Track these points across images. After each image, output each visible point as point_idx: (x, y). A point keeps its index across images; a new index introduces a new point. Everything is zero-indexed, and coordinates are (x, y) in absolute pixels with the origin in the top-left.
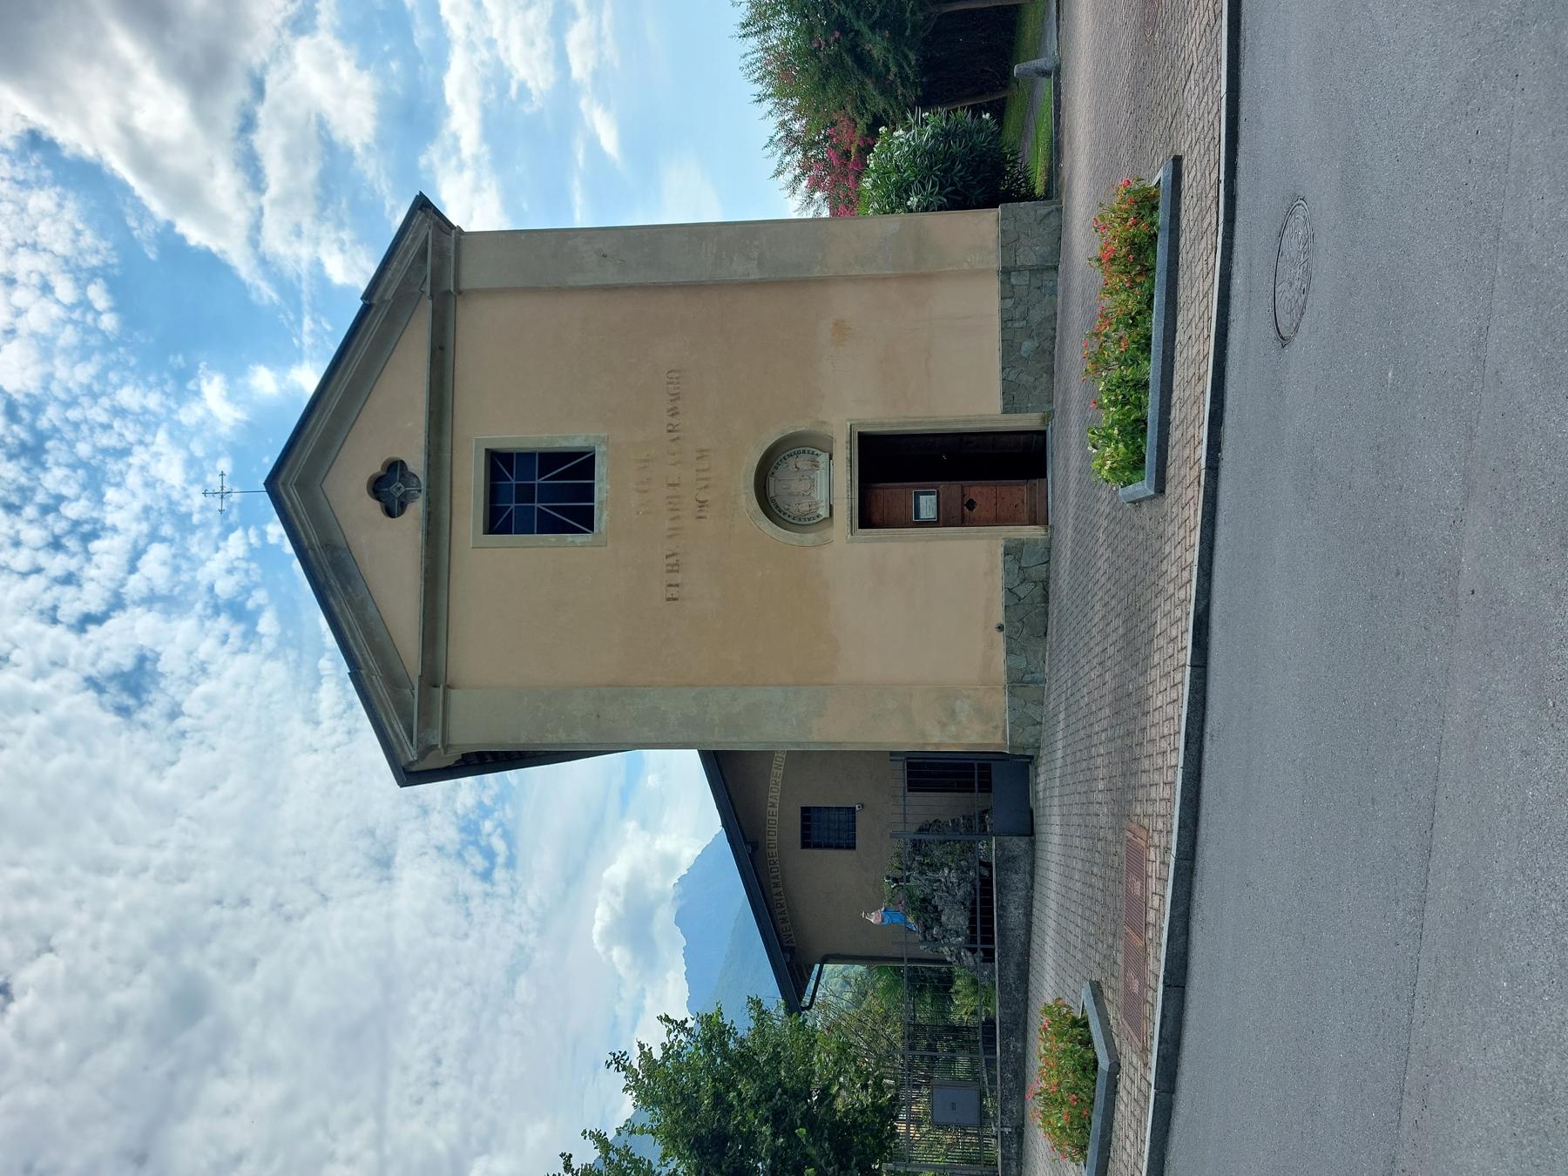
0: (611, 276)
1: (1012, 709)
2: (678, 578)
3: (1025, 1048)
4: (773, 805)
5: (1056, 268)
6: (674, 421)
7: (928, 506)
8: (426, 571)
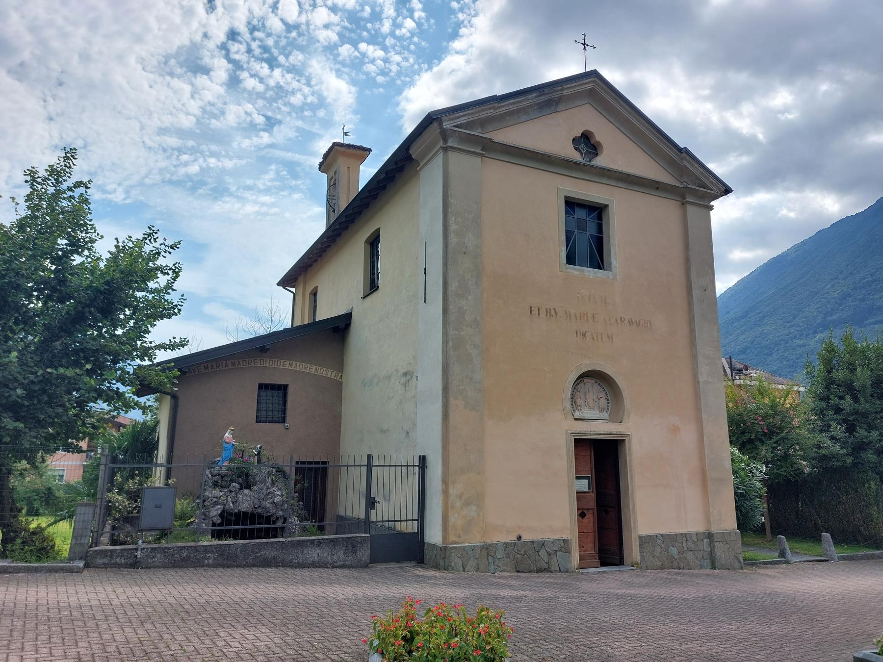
1: (473, 548)
3: (208, 566)
4: (291, 365)
5: (714, 567)
7: (583, 485)
8: (549, 156)
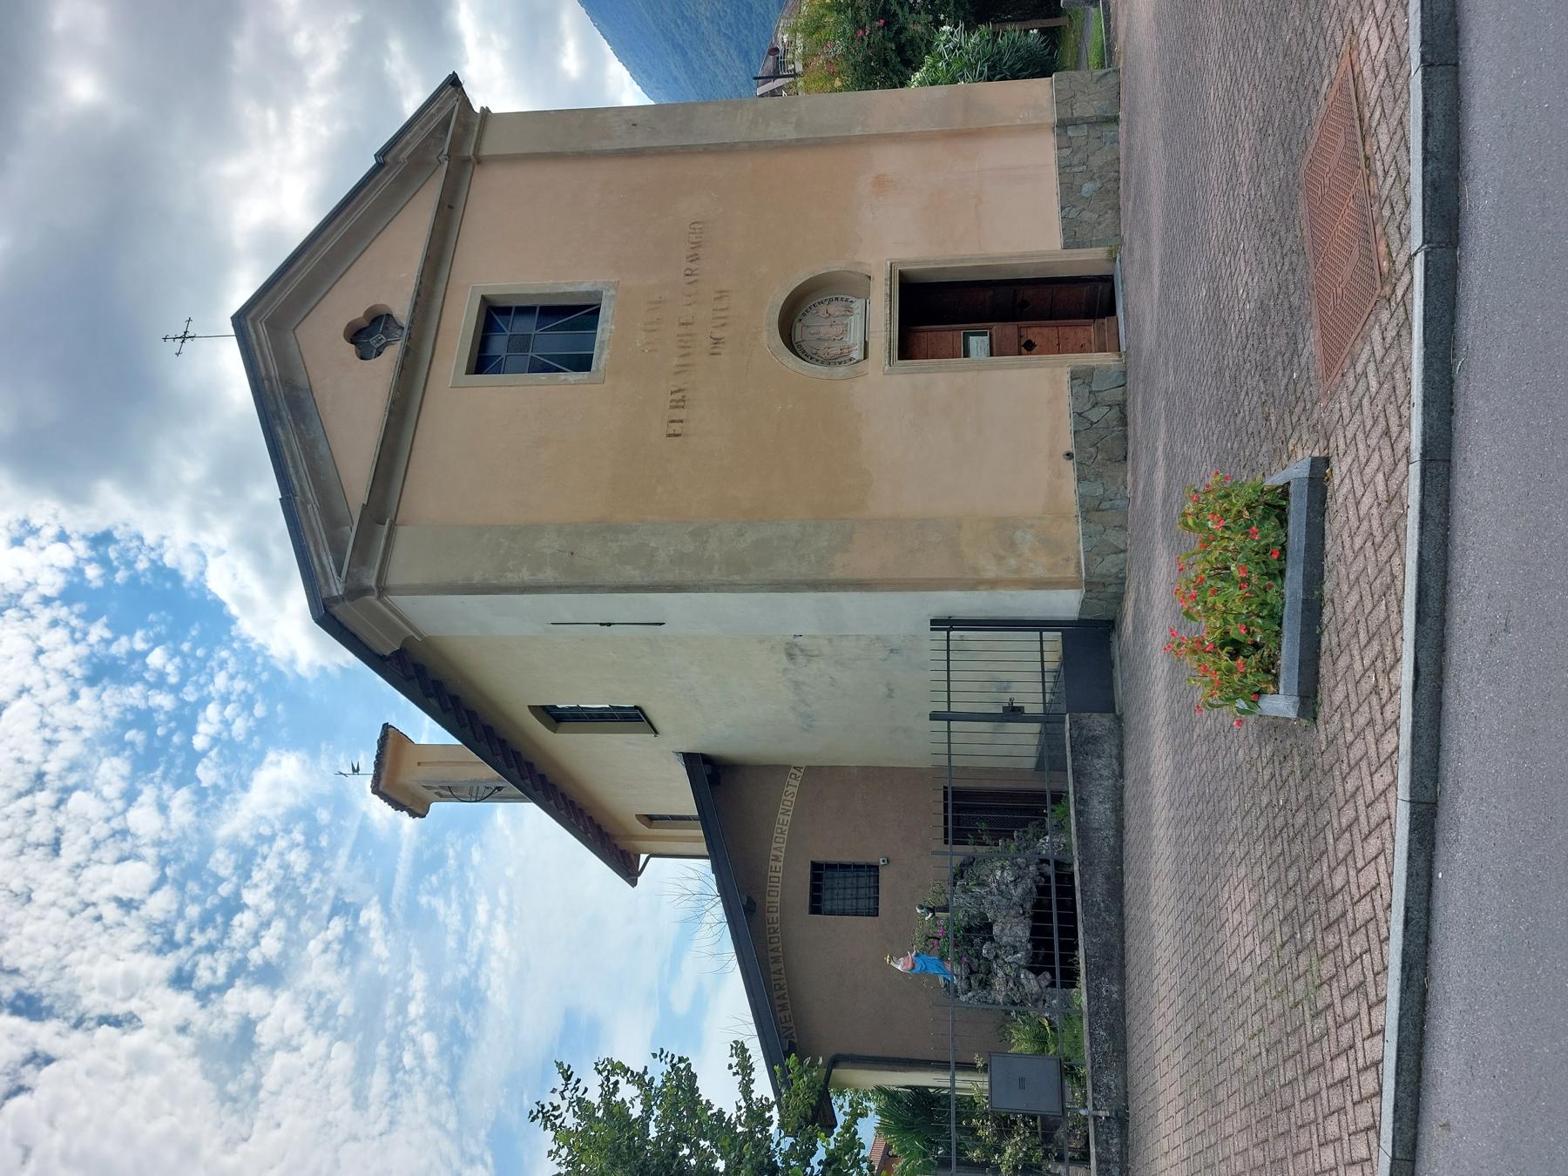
0: (639, 142)
1: (1087, 535)
2: (682, 414)
3: (1122, 992)
4: (777, 859)
5: (1116, 120)
6: (693, 266)
8: (393, 402)
